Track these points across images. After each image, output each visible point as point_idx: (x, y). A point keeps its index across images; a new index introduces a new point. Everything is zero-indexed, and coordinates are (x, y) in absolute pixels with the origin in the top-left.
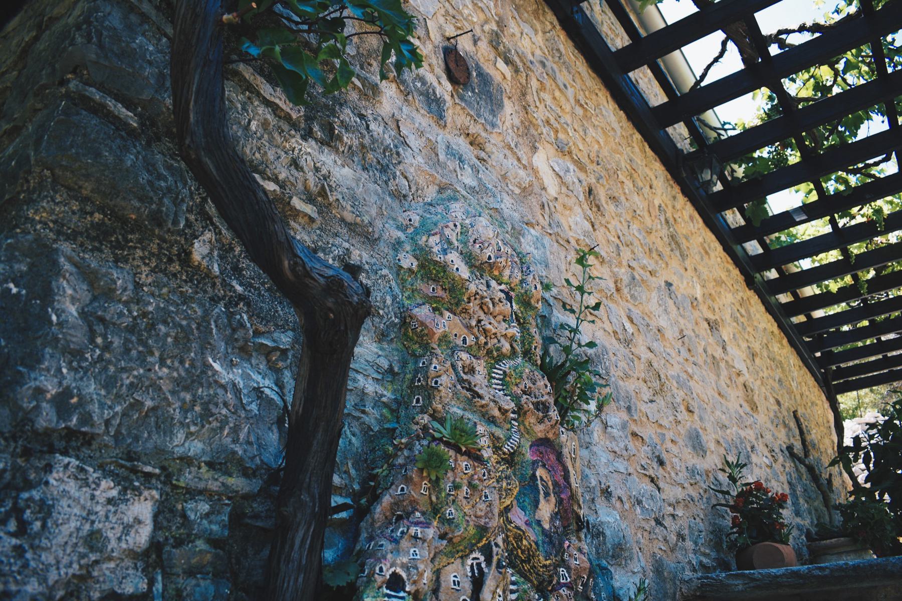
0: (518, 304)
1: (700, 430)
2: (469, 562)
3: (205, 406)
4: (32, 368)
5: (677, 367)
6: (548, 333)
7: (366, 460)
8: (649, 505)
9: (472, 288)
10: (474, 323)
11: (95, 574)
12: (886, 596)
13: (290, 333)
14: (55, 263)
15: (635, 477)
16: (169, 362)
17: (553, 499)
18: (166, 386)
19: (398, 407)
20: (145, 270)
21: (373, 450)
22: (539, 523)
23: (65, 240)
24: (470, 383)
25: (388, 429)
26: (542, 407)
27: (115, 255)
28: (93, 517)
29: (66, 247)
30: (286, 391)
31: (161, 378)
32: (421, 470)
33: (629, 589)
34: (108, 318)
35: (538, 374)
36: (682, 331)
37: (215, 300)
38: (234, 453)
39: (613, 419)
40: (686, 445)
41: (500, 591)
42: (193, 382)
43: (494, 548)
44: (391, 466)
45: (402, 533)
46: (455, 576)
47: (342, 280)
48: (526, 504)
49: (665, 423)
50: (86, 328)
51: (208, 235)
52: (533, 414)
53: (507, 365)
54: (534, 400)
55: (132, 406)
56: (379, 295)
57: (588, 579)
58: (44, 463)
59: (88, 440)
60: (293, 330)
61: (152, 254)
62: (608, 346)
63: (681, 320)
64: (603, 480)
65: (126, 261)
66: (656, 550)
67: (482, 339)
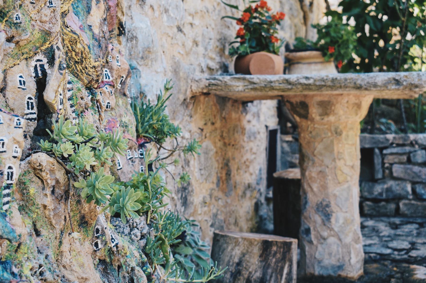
2: (33, 63)
8: (174, 14)
12: (347, 102)
33: (152, 86)
41: (61, 91)
43: (56, 51)
46: (21, 77)
48: (79, 9)
66: (176, 54)
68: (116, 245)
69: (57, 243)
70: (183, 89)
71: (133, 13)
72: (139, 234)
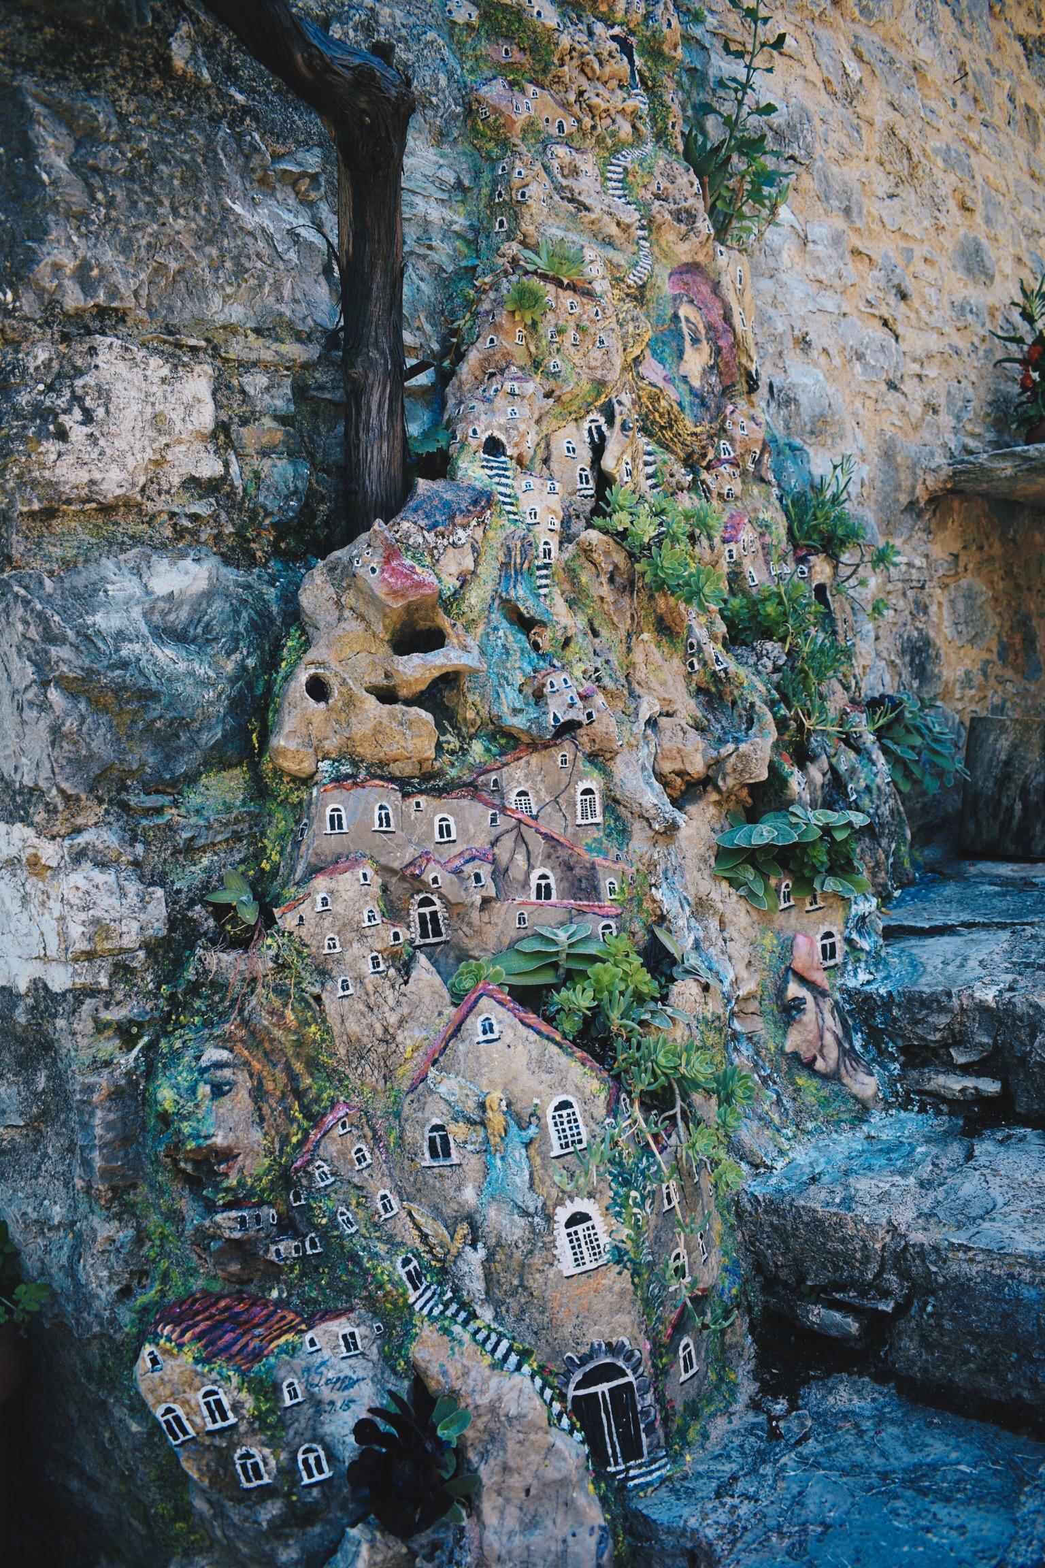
0: (641, 56)
1: (984, 241)
2: (586, 425)
3: (236, 259)
4: (41, 241)
5: (948, 134)
6: (704, 97)
7: (442, 312)
9: (565, 41)
10: (572, 97)
11: (169, 458)
13: (317, 150)
14: (24, 107)
15: (854, 319)
16: (182, 210)
17: (705, 347)
18: (187, 242)
19: (475, 236)
20: (122, 92)
21: (450, 298)
22: (685, 379)
23: (24, 72)
24: (572, 191)
25: (466, 268)
26: (685, 217)
27: (84, 81)
28: (152, 399)
29: (27, 82)
30: (326, 230)
31: (178, 233)
32: (513, 313)
34: (101, 166)
35: (679, 166)
36: (964, 64)
37: (215, 120)
38: (281, 315)
39: (817, 230)
40: (954, 267)
42: (215, 232)
44: (476, 314)
45: (496, 391)
47: (372, 69)
49: (914, 230)
50: (82, 183)
51: (185, 28)
52: (672, 228)
53: (629, 158)
54: (673, 207)
55: (156, 270)
56: (428, 73)
57: (762, 454)
58: (86, 346)
59: (121, 317)
60: (320, 145)
61: (125, 70)
62: (810, 105)
63: (964, 45)
64: (798, 324)
65: (99, 87)
67: (588, 122)
68: (725, 670)
69: (624, 648)
70: (906, 484)
71: (788, 362)
72: (769, 664)
